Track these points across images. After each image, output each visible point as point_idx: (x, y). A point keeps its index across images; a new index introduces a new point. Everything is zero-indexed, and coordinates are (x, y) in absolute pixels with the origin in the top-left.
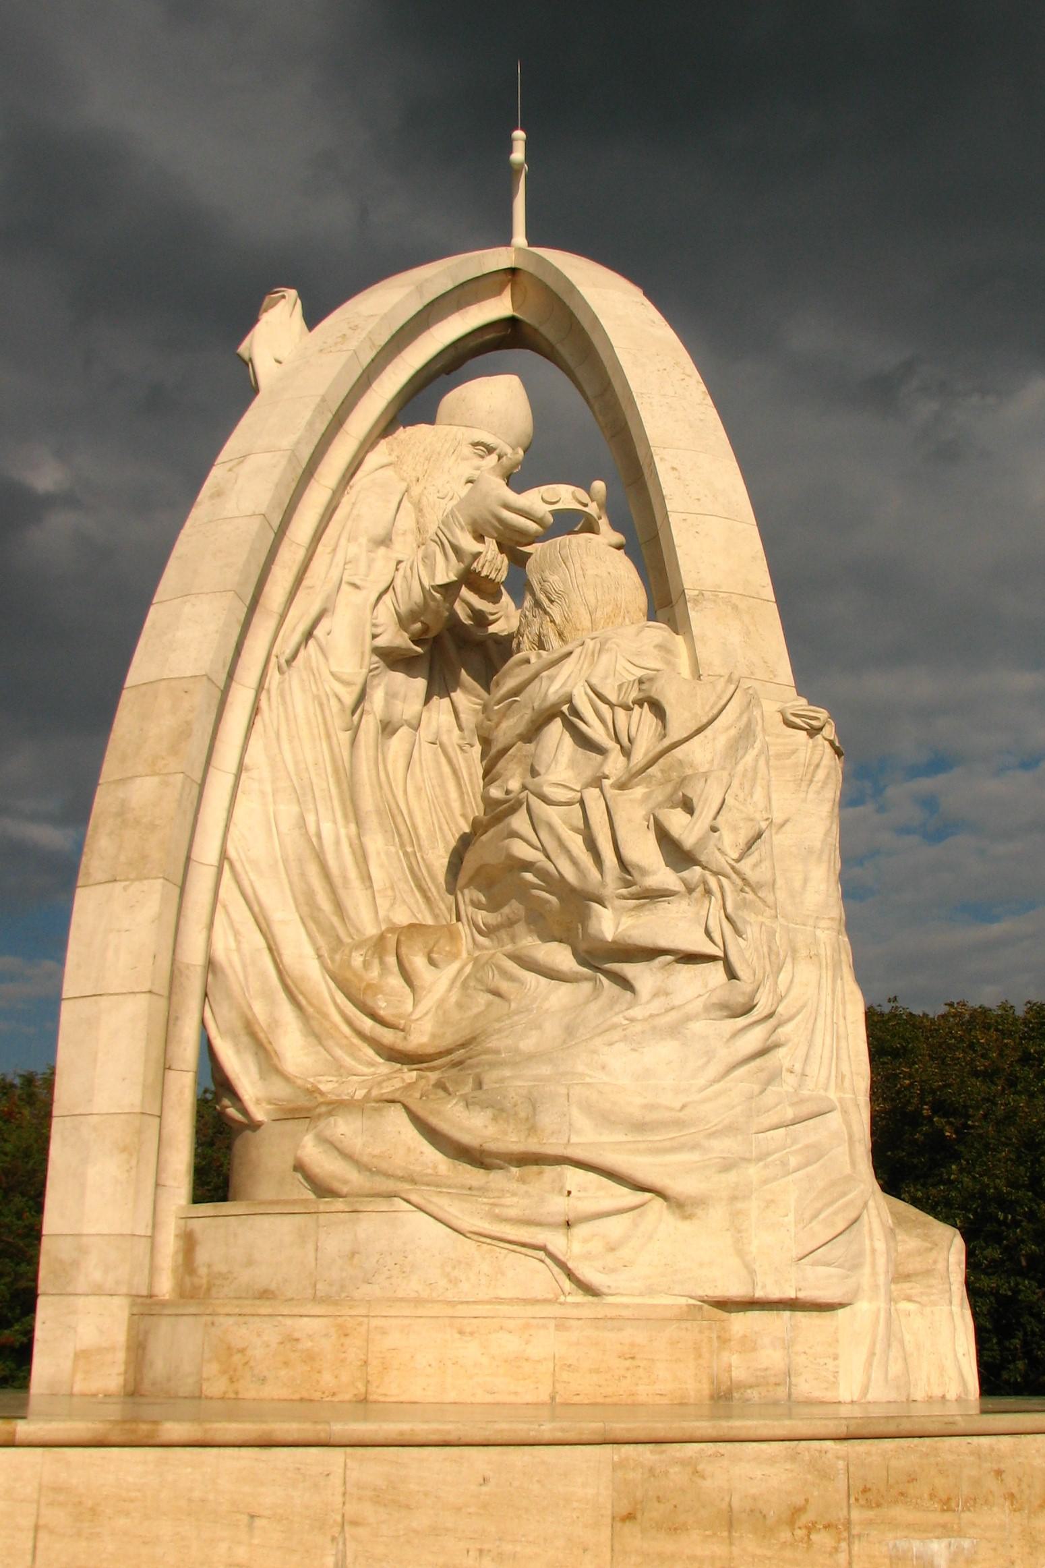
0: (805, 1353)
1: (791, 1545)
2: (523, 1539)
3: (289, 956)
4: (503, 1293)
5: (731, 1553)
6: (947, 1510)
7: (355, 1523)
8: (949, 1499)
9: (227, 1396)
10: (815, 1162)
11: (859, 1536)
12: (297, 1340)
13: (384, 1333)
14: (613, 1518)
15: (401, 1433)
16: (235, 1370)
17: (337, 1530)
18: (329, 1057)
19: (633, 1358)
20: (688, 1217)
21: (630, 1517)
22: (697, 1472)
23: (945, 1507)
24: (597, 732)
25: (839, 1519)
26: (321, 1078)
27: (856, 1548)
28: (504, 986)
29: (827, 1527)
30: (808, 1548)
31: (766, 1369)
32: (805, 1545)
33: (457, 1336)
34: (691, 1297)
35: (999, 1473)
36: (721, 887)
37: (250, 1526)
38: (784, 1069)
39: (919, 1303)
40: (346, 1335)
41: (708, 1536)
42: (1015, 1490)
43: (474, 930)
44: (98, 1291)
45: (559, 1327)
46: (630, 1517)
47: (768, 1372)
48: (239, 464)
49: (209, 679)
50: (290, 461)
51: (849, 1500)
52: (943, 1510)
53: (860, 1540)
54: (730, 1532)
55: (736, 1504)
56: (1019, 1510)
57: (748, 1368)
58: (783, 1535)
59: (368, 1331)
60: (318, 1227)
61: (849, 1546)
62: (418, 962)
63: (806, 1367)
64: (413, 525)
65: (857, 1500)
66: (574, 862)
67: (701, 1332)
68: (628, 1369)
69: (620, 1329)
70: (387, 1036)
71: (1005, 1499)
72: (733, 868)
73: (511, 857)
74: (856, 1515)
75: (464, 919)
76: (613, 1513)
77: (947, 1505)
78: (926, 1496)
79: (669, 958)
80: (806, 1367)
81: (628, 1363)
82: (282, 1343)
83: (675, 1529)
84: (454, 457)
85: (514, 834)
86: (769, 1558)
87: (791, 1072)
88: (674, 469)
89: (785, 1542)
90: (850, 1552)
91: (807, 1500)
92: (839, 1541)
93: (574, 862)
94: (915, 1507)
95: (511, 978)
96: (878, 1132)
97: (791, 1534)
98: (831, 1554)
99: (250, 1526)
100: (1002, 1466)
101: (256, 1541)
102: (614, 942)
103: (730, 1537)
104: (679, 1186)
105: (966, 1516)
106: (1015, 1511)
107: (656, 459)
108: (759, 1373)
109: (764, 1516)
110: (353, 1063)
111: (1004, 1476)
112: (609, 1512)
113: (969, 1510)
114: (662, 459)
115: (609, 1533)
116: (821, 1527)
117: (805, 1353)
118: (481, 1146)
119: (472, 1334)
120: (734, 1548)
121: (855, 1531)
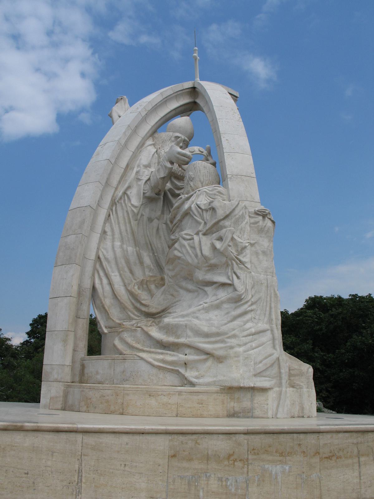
0: (257, 403)
1: (228, 466)
2: (139, 462)
3: (116, 286)
4: (166, 384)
5: (208, 467)
6: (281, 456)
7: (85, 455)
8: (282, 453)
10: (262, 346)
11: (251, 464)
12: (104, 396)
13: (128, 395)
14: (169, 456)
15: (100, 429)
16: (88, 404)
17: (79, 457)
18: (127, 314)
19: (202, 404)
20: (221, 362)
21: (174, 456)
22: (197, 443)
23: (281, 455)
24: (199, 220)
25: (244, 458)
26: (125, 320)
27: (250, 467)
29: (240, 460)
30: (234, 467)
31: (245, 408)
32: (233, 466)
33: (149, 396)
34: (221, 386)
35: (300, 445)
36: (232, 264)
37: (52, 455)
38: (253, 318)
39: (296, 388)
40: (118, 395)
41: (200, 462)
42: (305, 450)
43: (169, 277)
44: (56, 381)
45: (179, 395)
46: (174, 456)
47: (246, 409)
48: (104, 145)
49: (90, 207)
50: (117, 144)
51: (248, 452)
52: (280, 456)
53: (361, 441)
54: (207, 461)
55: (210, 453)
56: (306, 456)
57: (240, 407)
58: (225, 463)
59: (124, 394)
60: (115, 363)
61: (248, 467)
63: (258, 407)
64: (157, 161)
65: (251, 452)
66: (191, 256)
67: (224, 396)
68: (200, 407)
69: (198, 395)
70: (143, 309)
71: (302, 453)
72: (236, 257)
73: (175, 256)
74: (250, 457)
76: (169, 455)
77: (281, 454)
78: (274, 451)
79: (217, 285)
80: (258, 407)
81: (201, 405)
82: (100, 397)
83: (190, 460)
84: (170, 141)
85: (176, 249)
86: (221, 470)
87: (255, 319)
88: (227, 140)
89: (226, 465)
90: (248, 468)
91: (234, 452)
92: (244, 465)
93: (191, 256)
94: (270, 455)
95: (177, 291)
96: (16, 351)
97: (228, 462)
98: (241, 469)
99: (52, 455)
100: (301, 443)
101: (54, 459)
102: (202, 280)
103: (207, 463)
105: (288, 458)
106: (305, 456)
107: (222, 137)
108: (242, 409)
109: (219, 457)
110: (134, 316)
111: (301, 446)
112: (168, 454)
113: (289, 456)
114: (224, 137)
115: (167, 461)
116: (238, 460)
117: (257, 403)
118: (161, 340)
119: (153, 396)
120: (209, 466)
121: (250, 462)
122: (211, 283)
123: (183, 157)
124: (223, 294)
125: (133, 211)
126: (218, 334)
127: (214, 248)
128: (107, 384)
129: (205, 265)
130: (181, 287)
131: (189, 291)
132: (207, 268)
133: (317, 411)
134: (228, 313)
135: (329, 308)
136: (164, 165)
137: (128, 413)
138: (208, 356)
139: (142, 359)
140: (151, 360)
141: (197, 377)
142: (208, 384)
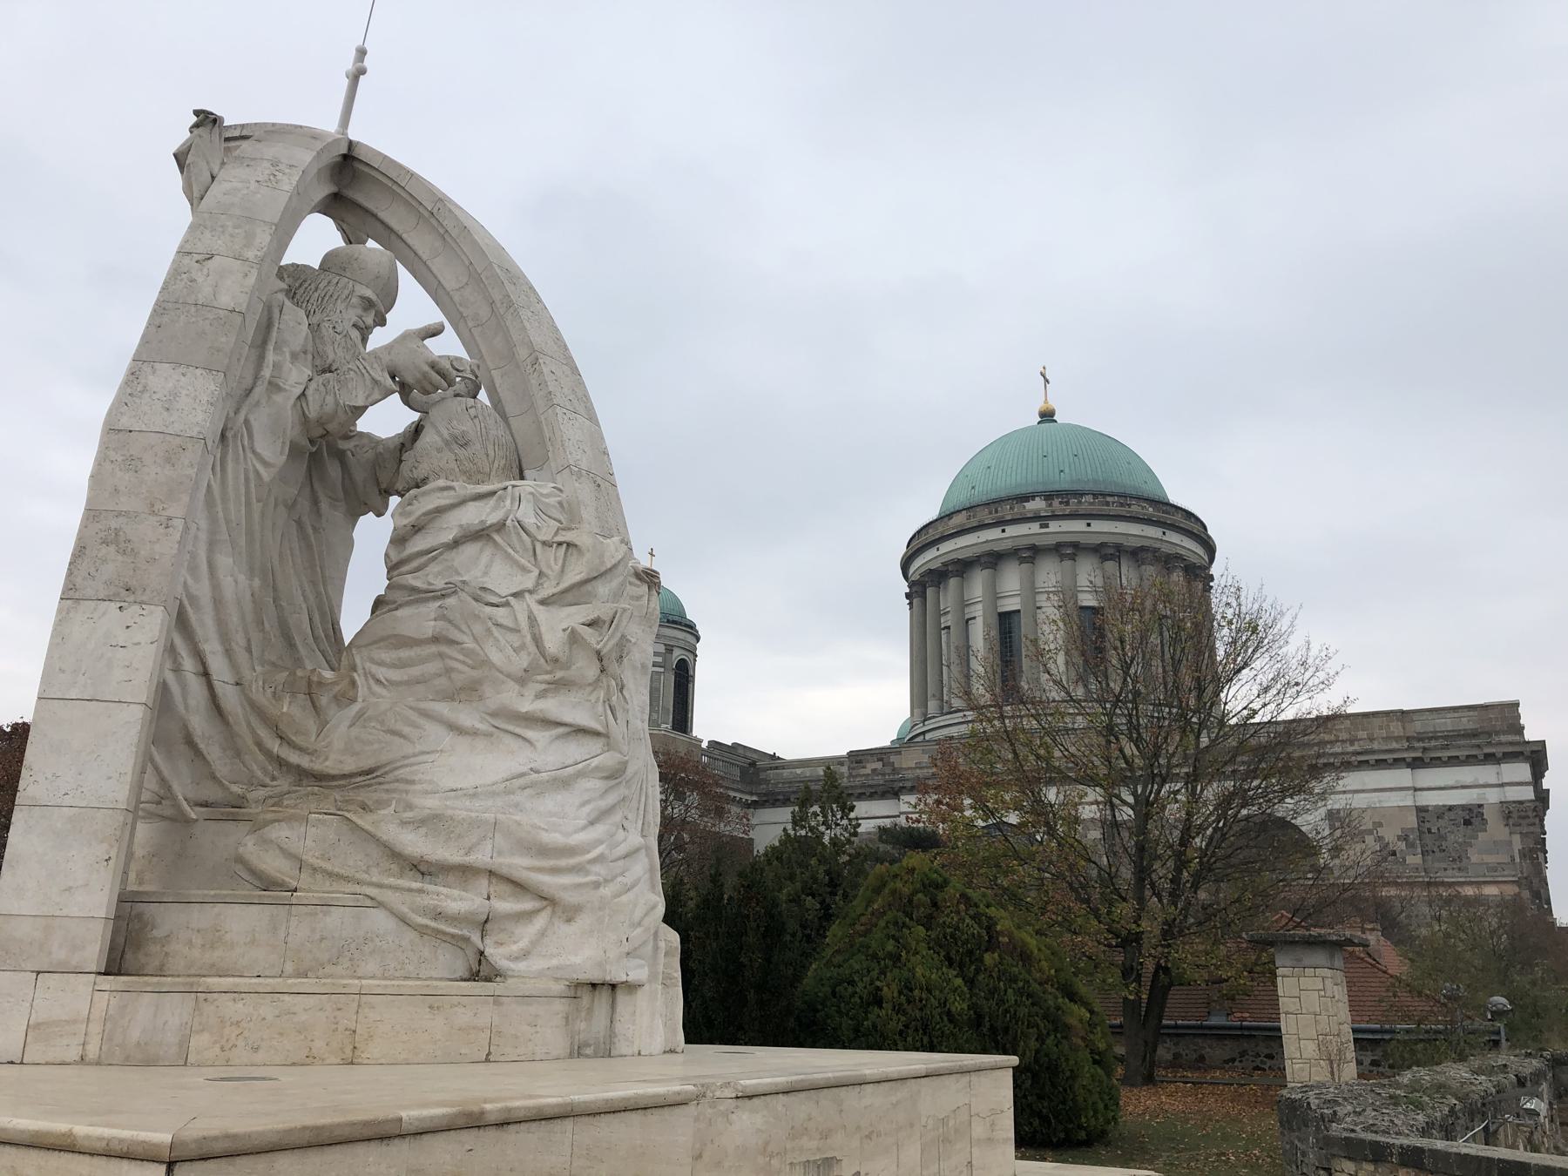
28: (406, 730)
70: (294, 758)
75: (360, 671)
79: (561, 730)
104: (570, 898)
124: (576, 751)
125: (257, 472)
126: (570, 851)
130: (426, 714)
132: (544, 686)
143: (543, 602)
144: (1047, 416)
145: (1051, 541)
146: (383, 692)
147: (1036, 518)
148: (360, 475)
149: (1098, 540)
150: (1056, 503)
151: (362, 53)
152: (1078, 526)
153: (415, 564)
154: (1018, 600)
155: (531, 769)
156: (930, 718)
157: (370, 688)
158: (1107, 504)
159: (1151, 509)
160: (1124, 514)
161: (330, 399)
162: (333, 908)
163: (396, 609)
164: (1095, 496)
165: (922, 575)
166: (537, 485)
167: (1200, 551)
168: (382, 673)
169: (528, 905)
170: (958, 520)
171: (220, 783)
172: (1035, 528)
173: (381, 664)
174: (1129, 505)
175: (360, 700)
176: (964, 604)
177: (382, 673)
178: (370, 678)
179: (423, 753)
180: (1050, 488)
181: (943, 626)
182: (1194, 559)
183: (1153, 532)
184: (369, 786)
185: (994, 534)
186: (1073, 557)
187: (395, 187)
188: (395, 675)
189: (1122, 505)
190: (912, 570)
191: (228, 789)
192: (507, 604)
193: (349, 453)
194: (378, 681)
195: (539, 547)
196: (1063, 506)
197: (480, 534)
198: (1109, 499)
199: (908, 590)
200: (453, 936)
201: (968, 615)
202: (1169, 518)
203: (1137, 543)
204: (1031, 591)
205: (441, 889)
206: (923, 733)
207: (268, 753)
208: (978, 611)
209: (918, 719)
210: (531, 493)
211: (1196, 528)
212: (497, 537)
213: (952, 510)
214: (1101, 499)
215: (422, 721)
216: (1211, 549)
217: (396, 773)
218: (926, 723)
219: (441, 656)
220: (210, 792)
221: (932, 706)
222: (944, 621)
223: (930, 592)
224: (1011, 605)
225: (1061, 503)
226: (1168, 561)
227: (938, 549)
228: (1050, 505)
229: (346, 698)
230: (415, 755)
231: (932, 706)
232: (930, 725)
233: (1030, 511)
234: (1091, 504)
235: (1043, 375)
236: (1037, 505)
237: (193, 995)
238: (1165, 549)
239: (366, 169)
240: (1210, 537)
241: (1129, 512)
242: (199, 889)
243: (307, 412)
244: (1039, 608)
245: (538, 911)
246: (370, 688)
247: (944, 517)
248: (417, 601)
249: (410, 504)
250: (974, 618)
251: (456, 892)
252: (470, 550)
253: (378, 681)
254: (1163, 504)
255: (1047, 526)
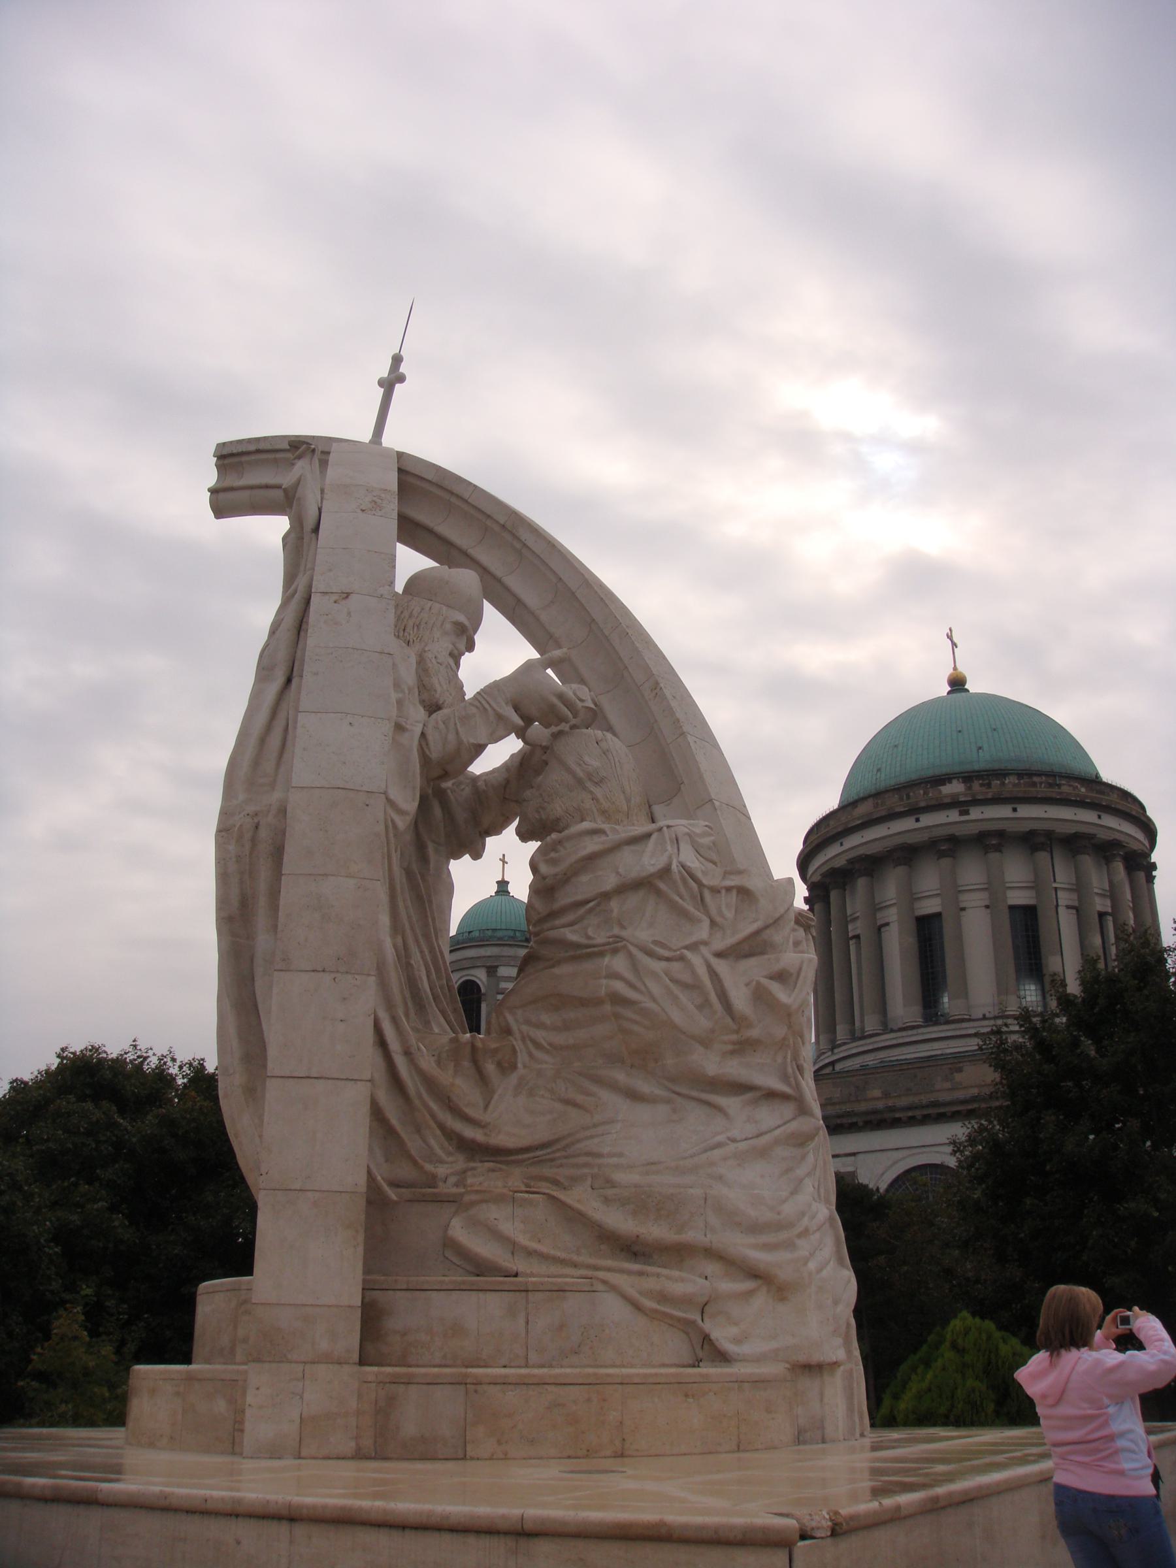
9: (495, 1457)
20: (783, 1299)
28: (580, 1098)
40: (604, 1400)
62: (490, 1068)
70: (469, 1132)
75: (518, 1035)
79: (758, 1094)
95: (588, 1094)
104: (784, 1274)
122: (739, 1088)
123: (566, 709)
125: (392, 821)
126: (779, 1226)
127: (760, 996)
128: (505, 1367)
129: (726, 1038)
130: (599, 1081)
131: (634, 1096)
132: (730, 1047)
133: (871, 1426)
134: (788, 1170)
135: (63, 1111)
136: (494, 710)
137: (637, 1450)
138: (760, 1282)
139: (613, 1288)
140: (632, 1293)
141: (738, 1341)
142: (758, 1359)
143: (719, 955)
144: (957, 684)
145: (974, 829)
146: (546, 1057)
147: (954, 804)
148: (461, 816)
149: (1026, 827)
150: (976, 785)
151: (397, 360)
152: (1004, 811)
153: (570, 917)
154: (938, 901)
155: (729, 1139)
156: (840, 1045)
157: (531, 1055)
158: (1034, 784)
159: (1083, 790)
160: (1054, 795)
161: (451, 737)
162: (568, 1293)
163: (553, 966)
164: (1020, 775)
165: (824, 875)
166: (690, 825)
167: (1140, 835)
168: (540, 1035)
169: (749, 1285)
170: (863, 809)
171: (415, 1163)
172: (953, 816)
173: (540, 1026)
174: (1059, 786)
175: (520, 1065)
176: (875, 908)
177: (540, 1035)
178: (529, 1042)
179: (604, 1123)
180: (968, 768)
181: (850, 935)
182: (1135, 846)
183: (1088, 816)
184: (552, 1160)
185: (907, 824)
186: (998, 848)
187: (453, 500)
188: (560, 1039)
189: (1050, 785)
190: (811, 869)
191: (422, 1168)
192: (682, 958)
193: (449, 791)
194: (538, 1046)
195: (707, 895)
196: (984, 789)
197: (643, 884)
198: (1036, 779)
199: (807, 895)
200: (679, 1320)
201: (881, 917)
202: (1105, 800)
203: (1072, 829)
204: (953, 891)
205: (660, 1270)
206: (833, 1063)
207: (442, 1127)
208: (892, 915)
209: (824, 1046)
210: (688, 834)
211: (1135, 811)
212: (662, 886)
213: (856, 798)
214: (1026, 780)
215: (594, 1088)
216: (1150, 831)
217: (578, 1146)
218: (836, 1051)
219: (617, 1016)
220: (405, 1172)
221: (841, 1031)
222: (853, 929)
223: (834, 895)
224: (930, 907)
225: (982, 785)
226: (1106, 850)
227: (841, 844)
228: (970, 788)
229: (507, 1067)
230: (595, 1126)
231: (841, 1031)
232: (840, 1053)
233: (946, 796)
234: (1015, 785)
235: (950, 637)
236: (950, 789)
237: (462, 1387)
238: (1103, 835)
239: (418, 483)
240: (1149, 820)
241: (1060, 793)
242: (460, 1276)
243: (428, 753)
244: (963, 909)
245: (750, 1293)
246: (531, 1055)
247: (847, 806)
248: (574, 958)
249: (554, 850)
250: (887, 924)
251: (676, 1273)
252: (633, 900)
253: (538, 1046)
254: (1095, 782)
255: (967, 813)
